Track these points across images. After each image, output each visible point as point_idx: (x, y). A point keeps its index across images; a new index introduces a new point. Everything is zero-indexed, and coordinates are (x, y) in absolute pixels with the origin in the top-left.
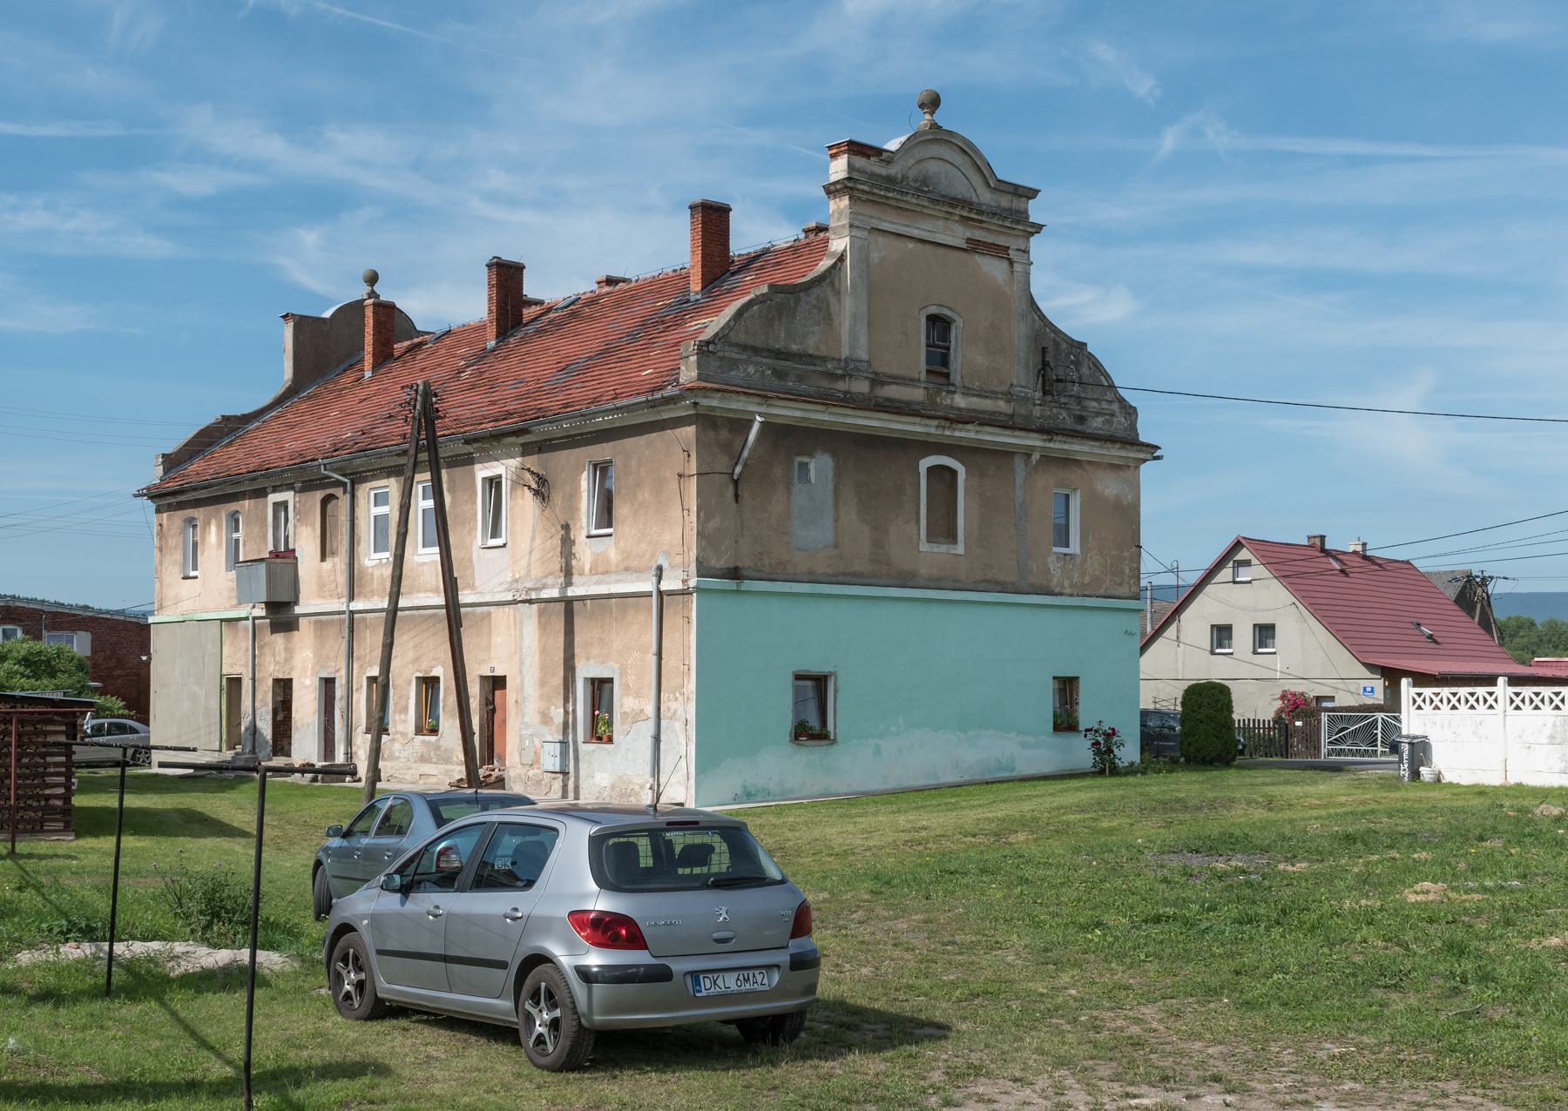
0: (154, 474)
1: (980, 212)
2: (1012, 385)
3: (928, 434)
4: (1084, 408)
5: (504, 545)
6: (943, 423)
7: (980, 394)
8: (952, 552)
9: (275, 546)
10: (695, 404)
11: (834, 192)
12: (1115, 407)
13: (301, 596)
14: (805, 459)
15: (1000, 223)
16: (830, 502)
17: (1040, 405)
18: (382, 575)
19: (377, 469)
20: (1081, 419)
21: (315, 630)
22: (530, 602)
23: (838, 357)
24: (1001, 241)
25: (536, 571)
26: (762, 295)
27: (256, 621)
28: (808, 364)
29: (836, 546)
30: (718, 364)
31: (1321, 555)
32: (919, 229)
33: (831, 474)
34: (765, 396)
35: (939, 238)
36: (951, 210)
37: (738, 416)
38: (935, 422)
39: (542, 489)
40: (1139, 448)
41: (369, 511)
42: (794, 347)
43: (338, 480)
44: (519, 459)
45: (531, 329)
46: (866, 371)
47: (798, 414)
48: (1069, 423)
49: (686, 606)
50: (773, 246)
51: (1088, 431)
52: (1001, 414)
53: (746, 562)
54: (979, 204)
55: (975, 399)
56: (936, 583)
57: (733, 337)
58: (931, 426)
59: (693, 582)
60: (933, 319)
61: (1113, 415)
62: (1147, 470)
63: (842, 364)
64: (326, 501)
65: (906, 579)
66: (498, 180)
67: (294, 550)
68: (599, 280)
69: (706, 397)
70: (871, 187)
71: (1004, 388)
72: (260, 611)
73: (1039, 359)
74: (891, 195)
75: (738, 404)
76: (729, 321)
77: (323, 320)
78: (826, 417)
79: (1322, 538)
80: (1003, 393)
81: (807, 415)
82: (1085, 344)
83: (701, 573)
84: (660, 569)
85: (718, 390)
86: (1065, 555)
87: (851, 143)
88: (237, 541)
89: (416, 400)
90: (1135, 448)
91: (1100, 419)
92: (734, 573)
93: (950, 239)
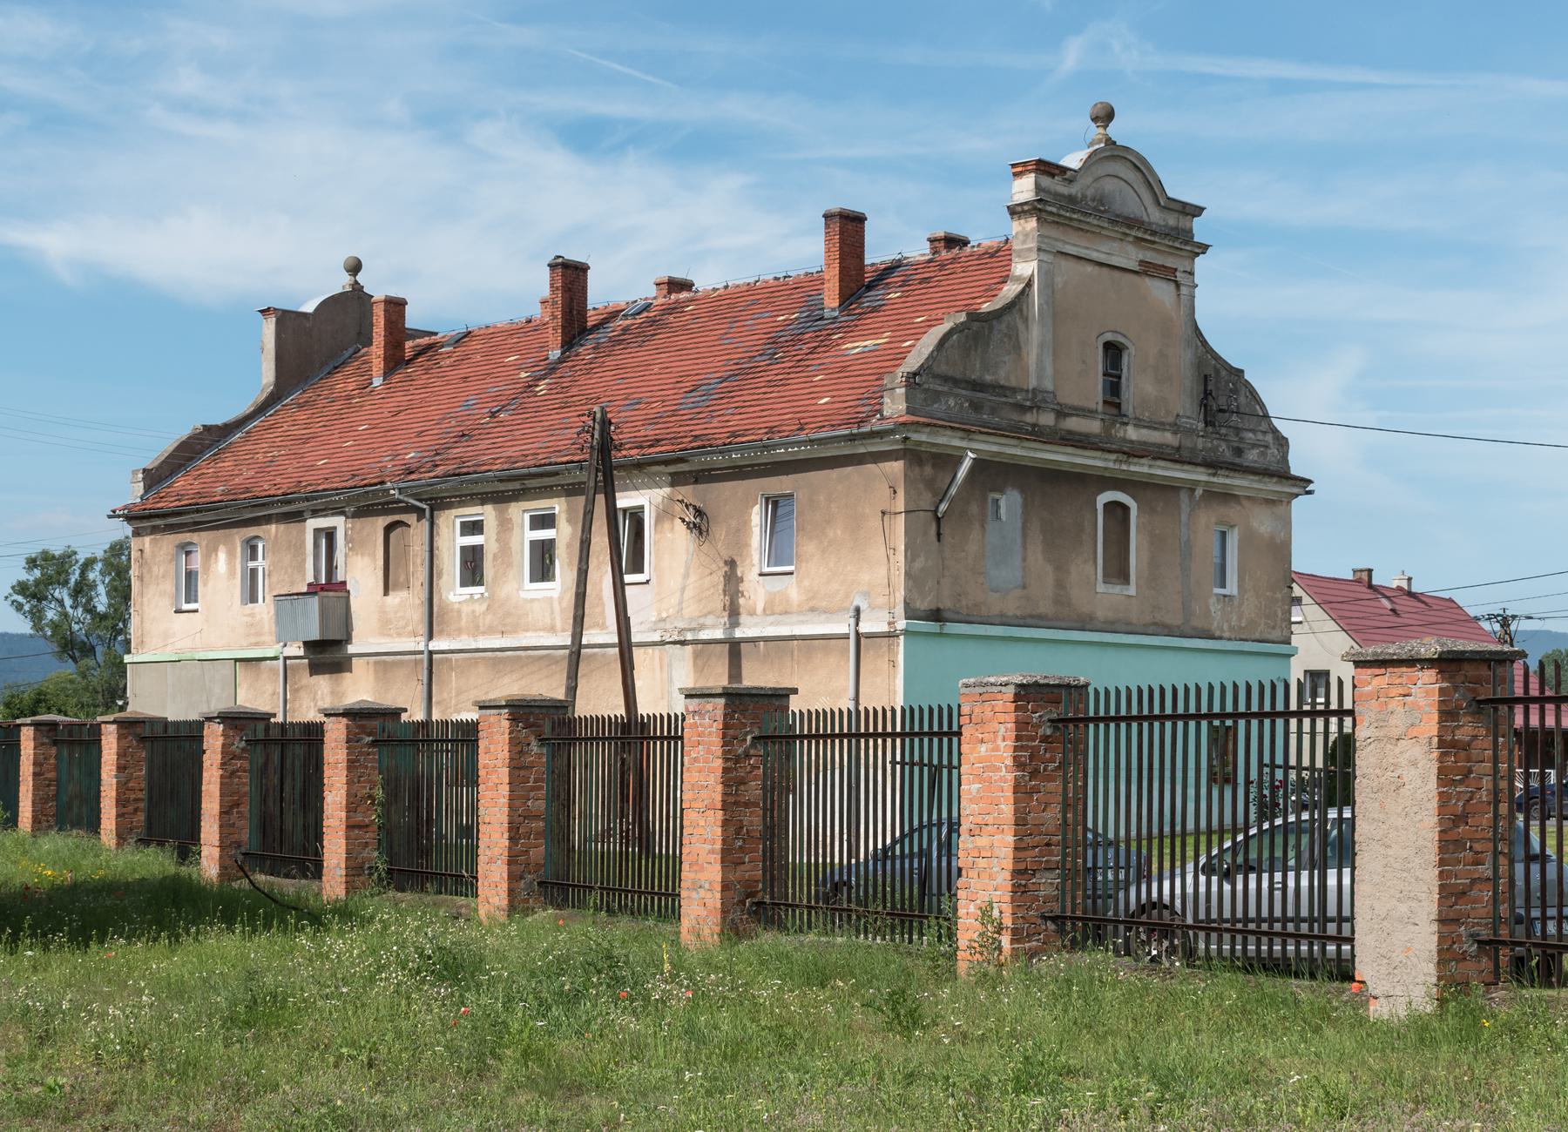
0: (133, 493)
1: (1154, 233)
2: (1178, 415)
3: (1106, 469)
4: (1242, 440)
5: (648, 582)
6: (1121, 457)
7: (1152, 426)
8: (1125, 593)
9: (316, 577)
10: (906, 438)
11: (1019, 213)
12: (1269, 438)
13: (354, 634)
14: (997, 496)
15: (1171, 243)
16: (1019, 540)
17: (1202, 436)
18: (473, 612)
19: (466, 496)
20: (1239, 452)
21: (376, 671)
22: (683, 643)
23: (1025, 388)
24: (1170, 262)
25: (691, 610)
26: (962, 323)
27: (288, 662)
28: (1000, 396)
29: (1024, 587)
30: (923, 396)
31: (1369, 591)
32: (1098, 251)
33: (1019, 511)
34: (969, 431)
35: (1115, 261)
36: (1128, 232)
37: (940, 451)
38: (1113, 457)
39: (700, 524)
40: (1293, 482)
41: (454, 541)
42: (988, 378)
43: (413, 506)
44: (667, 490)
45: (602, 336)
46: (1052, 403)
47: (995, 448)
48: (1228, 456)
49: (891, 650)
50: (906, 258)
51: (1245, 464)
52: (1168, 446)
53: (946, 604)
54: (1150, 223)
55: (1144, 431)
56: (1110, 627)
57: (936, 369)
58: (1110, 460)
59: (901, 624)
60: (1109, 346)
61: (1267, 447)
62: (1299, 505)
63: (1030, 395)
64: (389, 529)
65: (1085, 623)
66: (189, 82)
67: (344, 583)
68: (658, 281)
69: (916, 432)
70: (1058, 209)
71: (1171, 419)
72: (296, 650)
73: (1202, 388)
74: (1075, 216)
75: (948, 440)
76: (933, 351)
77: (305, 315)
78: (1019, 452)
79: (1370, 571)
80: (1170, 425)
81: (1032, 454)
82: (1242, 371)
83: (910, 614)
84: (858, 611)
85: (929, 425)
86: (1225, 596)
87: (1040, 162)
88: (254, 572)
89: (594, 429)
90: (1291, 482)
91: (1255, 452)
92: (936, 615)
93: (1125, 261)
